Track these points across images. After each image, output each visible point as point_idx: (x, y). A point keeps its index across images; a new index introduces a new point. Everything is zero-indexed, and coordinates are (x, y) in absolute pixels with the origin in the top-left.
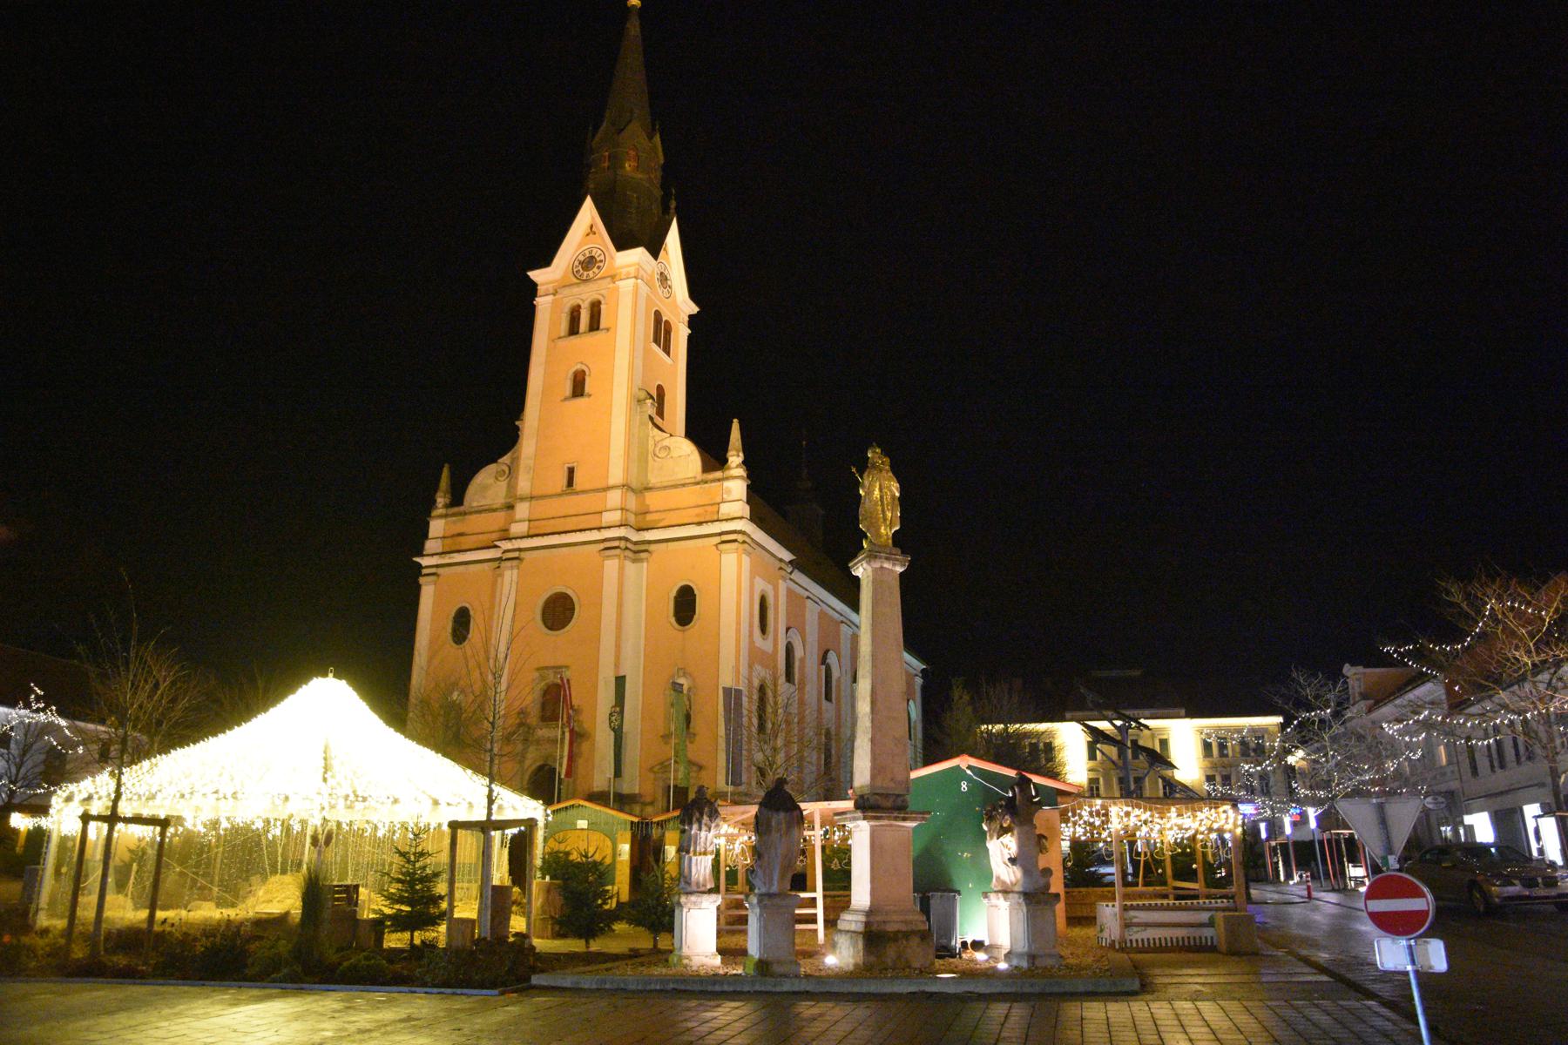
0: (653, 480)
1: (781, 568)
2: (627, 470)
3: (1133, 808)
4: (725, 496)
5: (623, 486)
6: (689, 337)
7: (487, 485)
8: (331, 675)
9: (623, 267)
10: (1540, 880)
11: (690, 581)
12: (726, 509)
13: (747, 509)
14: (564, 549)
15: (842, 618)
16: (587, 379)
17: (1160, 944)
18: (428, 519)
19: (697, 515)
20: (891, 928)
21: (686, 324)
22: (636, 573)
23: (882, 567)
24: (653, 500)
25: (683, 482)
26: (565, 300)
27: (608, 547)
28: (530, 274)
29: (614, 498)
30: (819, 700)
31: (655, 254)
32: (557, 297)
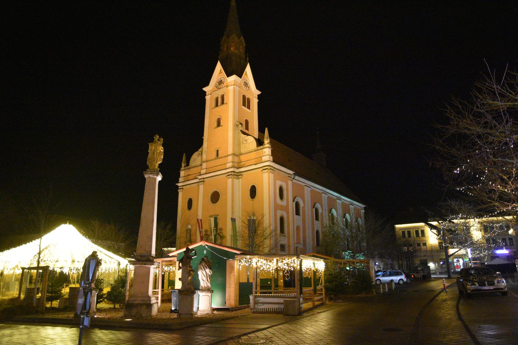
0: (243, 151)
1: (289, 177)
2: (234, 149)
3: (261, 259)
4: (264, 154)
5: (232, 154)
6: (258, 102)
7: (195, 159)
8: (68, 223)
9: (230, 82)
10: (486, 283)
11: (255, 184)
12: (264, 158)
13: (271, 158)
14: (216, 177)
15: (322, 192)
16: (221, 120)
17: (266, 310)
18: (144, 172)
19: (256, 162)
20: (136, 302)
21: (257, 98)
22: (238, 182)
23: (149, 177)
24: (243, 158)
25: (250, 151)
26: (214, 96)
27: (229, 175)
28: (203, 89)
29: (230, 158)
30: (312, 219)
31: (240, 76)
32: (212, 95)
